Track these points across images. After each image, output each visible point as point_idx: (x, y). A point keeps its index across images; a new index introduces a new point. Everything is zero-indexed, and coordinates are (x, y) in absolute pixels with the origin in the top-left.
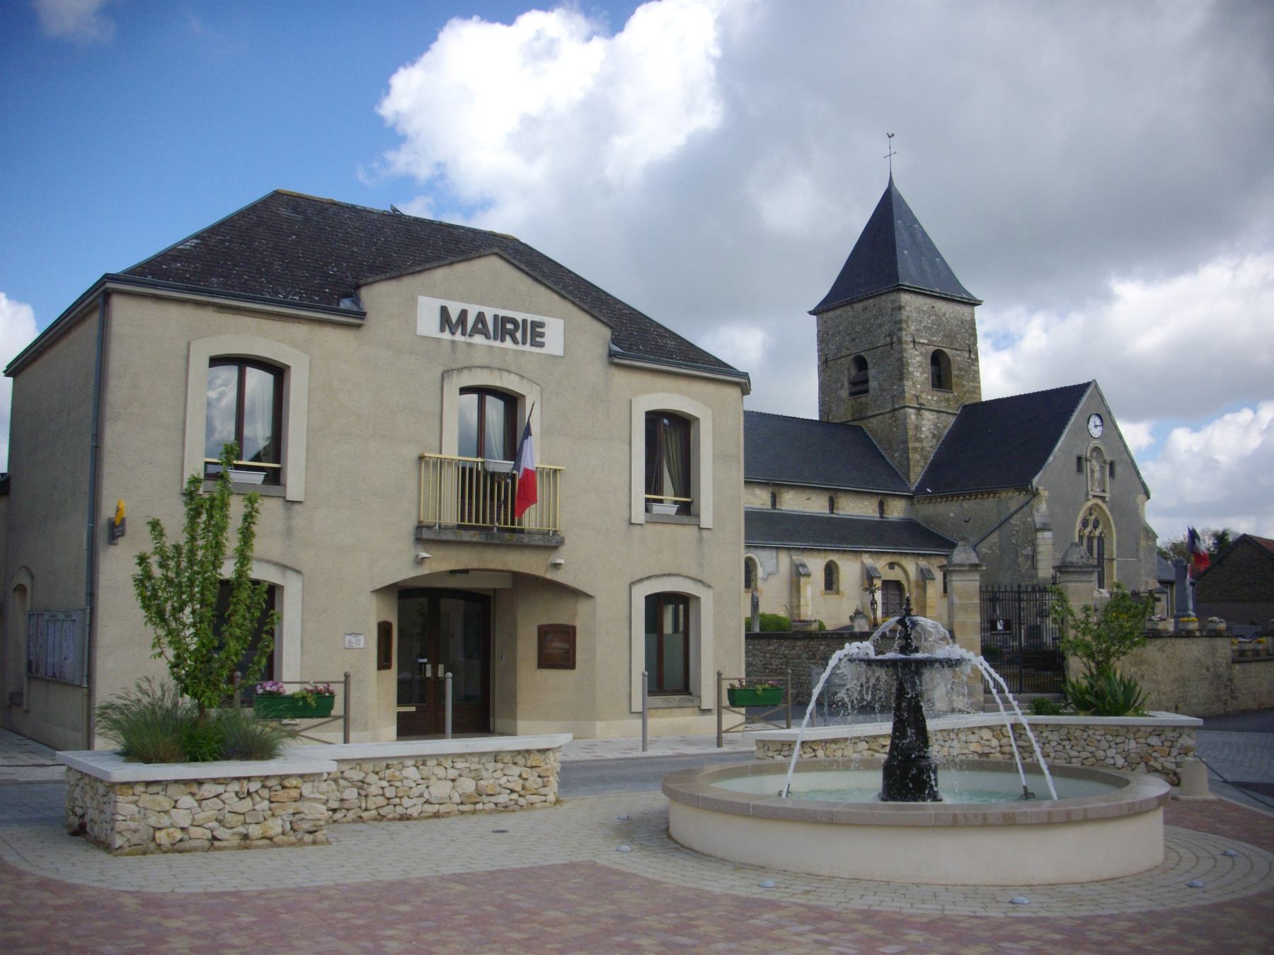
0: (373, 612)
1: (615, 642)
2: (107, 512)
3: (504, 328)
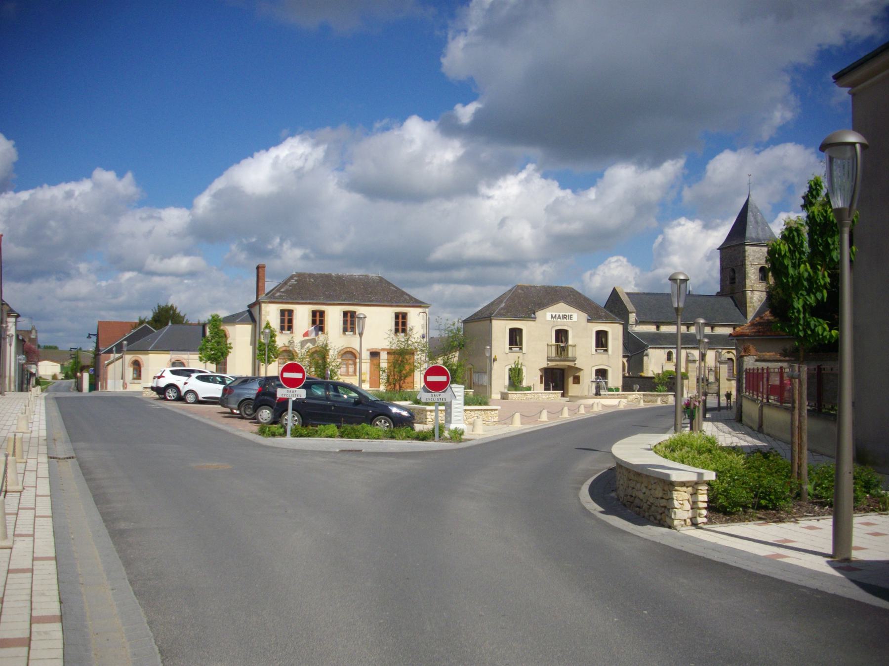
0: (539, 373)
1: (588, 376)
2: (493, 357)
3: (565, 317)
